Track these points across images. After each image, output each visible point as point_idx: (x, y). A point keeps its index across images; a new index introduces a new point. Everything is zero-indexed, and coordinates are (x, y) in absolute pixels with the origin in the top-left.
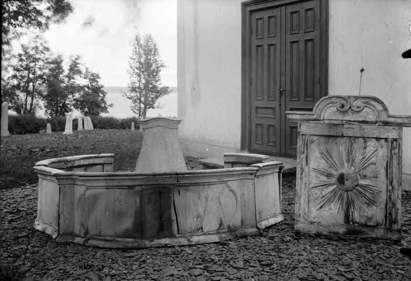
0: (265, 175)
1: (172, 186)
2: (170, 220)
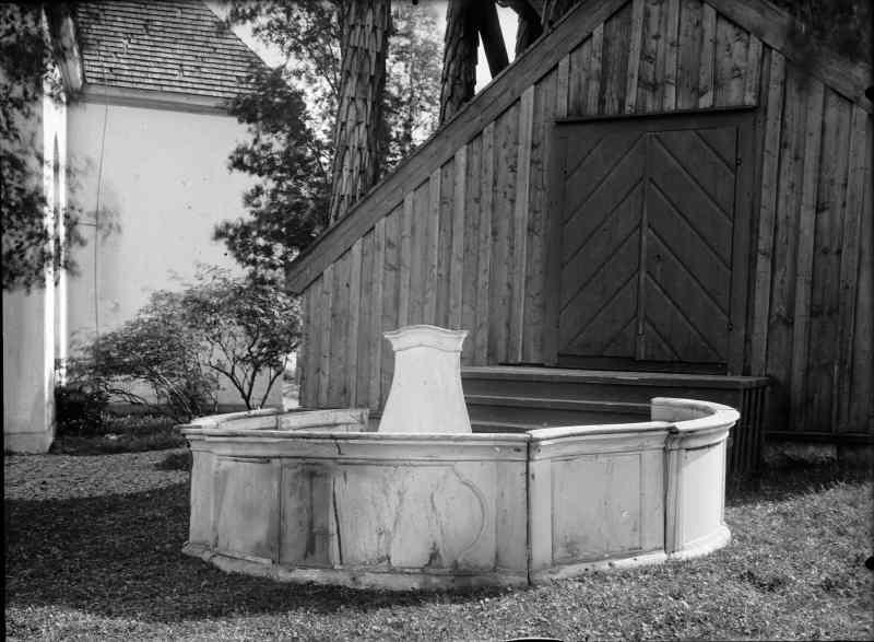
0: (709, 446)
1: (330, 463)
2: (326, 535)
